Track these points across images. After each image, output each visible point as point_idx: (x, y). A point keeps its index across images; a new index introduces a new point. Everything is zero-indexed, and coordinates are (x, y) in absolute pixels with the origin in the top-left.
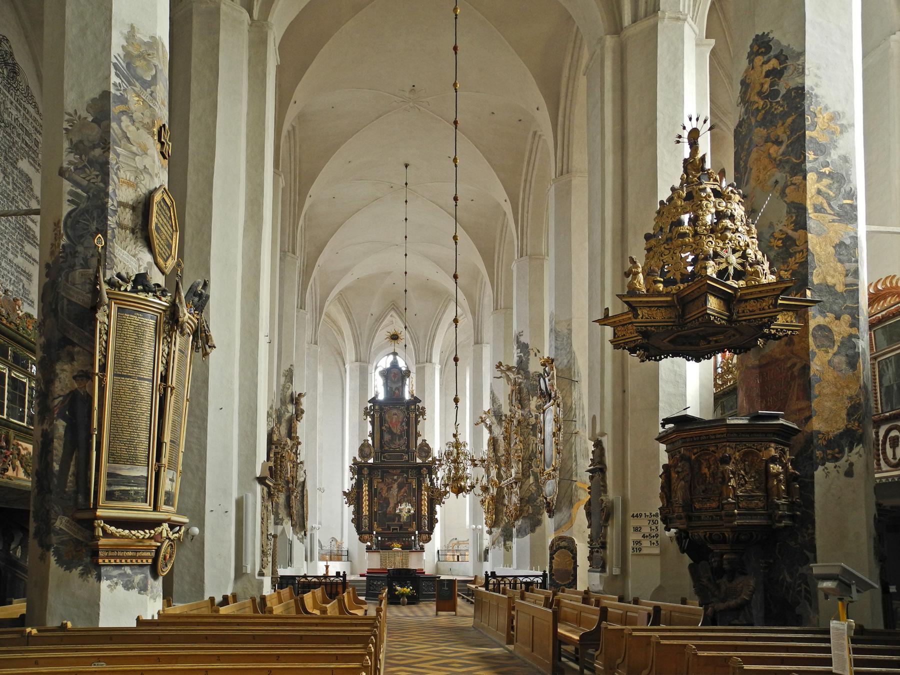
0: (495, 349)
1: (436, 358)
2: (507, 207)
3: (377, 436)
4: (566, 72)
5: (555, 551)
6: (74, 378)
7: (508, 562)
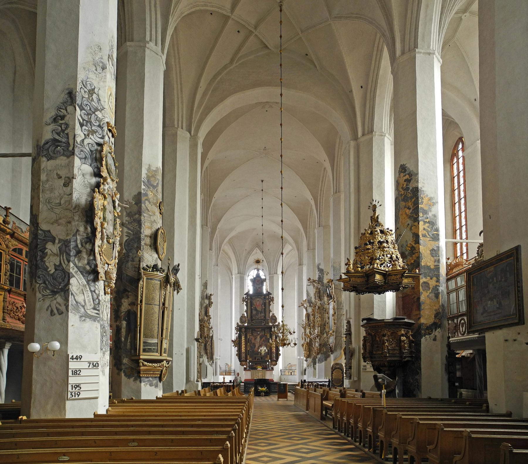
2: (313, 202)
3: (249, 312)
4: (337, 146)
6: (129, 305)
7: (314, 375)
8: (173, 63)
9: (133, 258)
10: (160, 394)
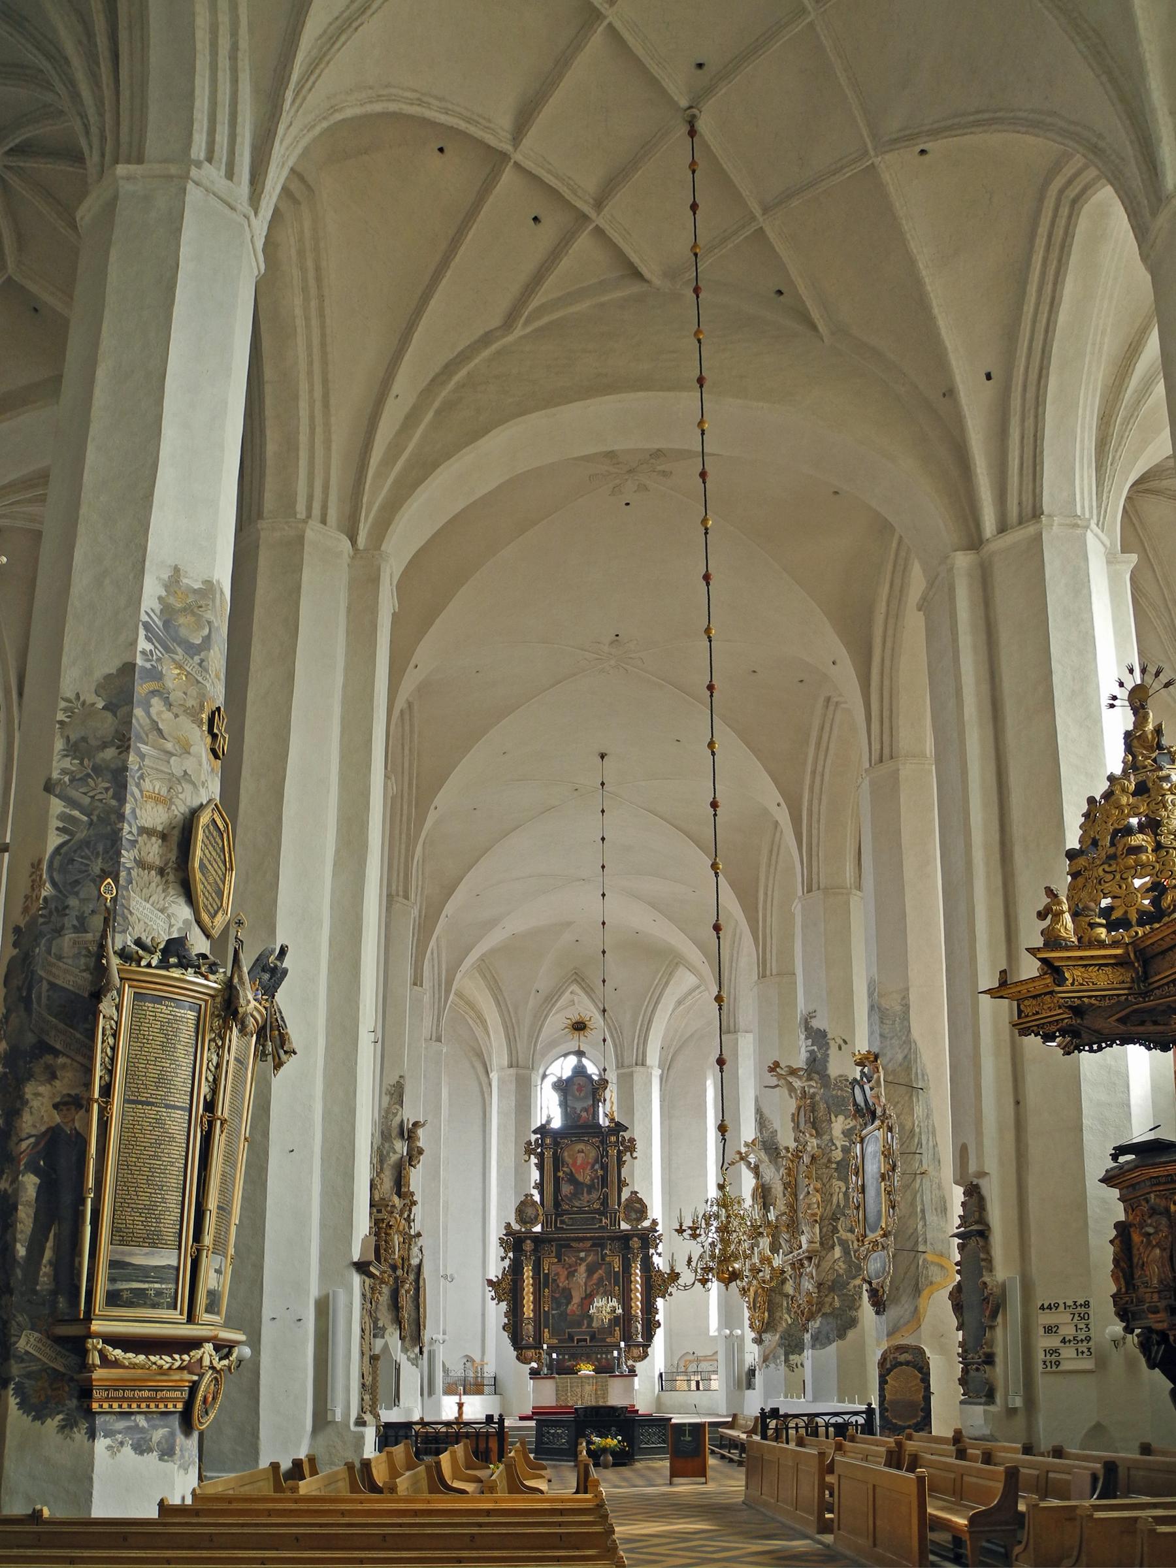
0: (762, 1041)
1: (653, 1057)
2: (783, 816)
3: (549, 1188)
5: (889, 1371)
8: (298, 312)
9: (81, 919)
10: (181, 1486)
